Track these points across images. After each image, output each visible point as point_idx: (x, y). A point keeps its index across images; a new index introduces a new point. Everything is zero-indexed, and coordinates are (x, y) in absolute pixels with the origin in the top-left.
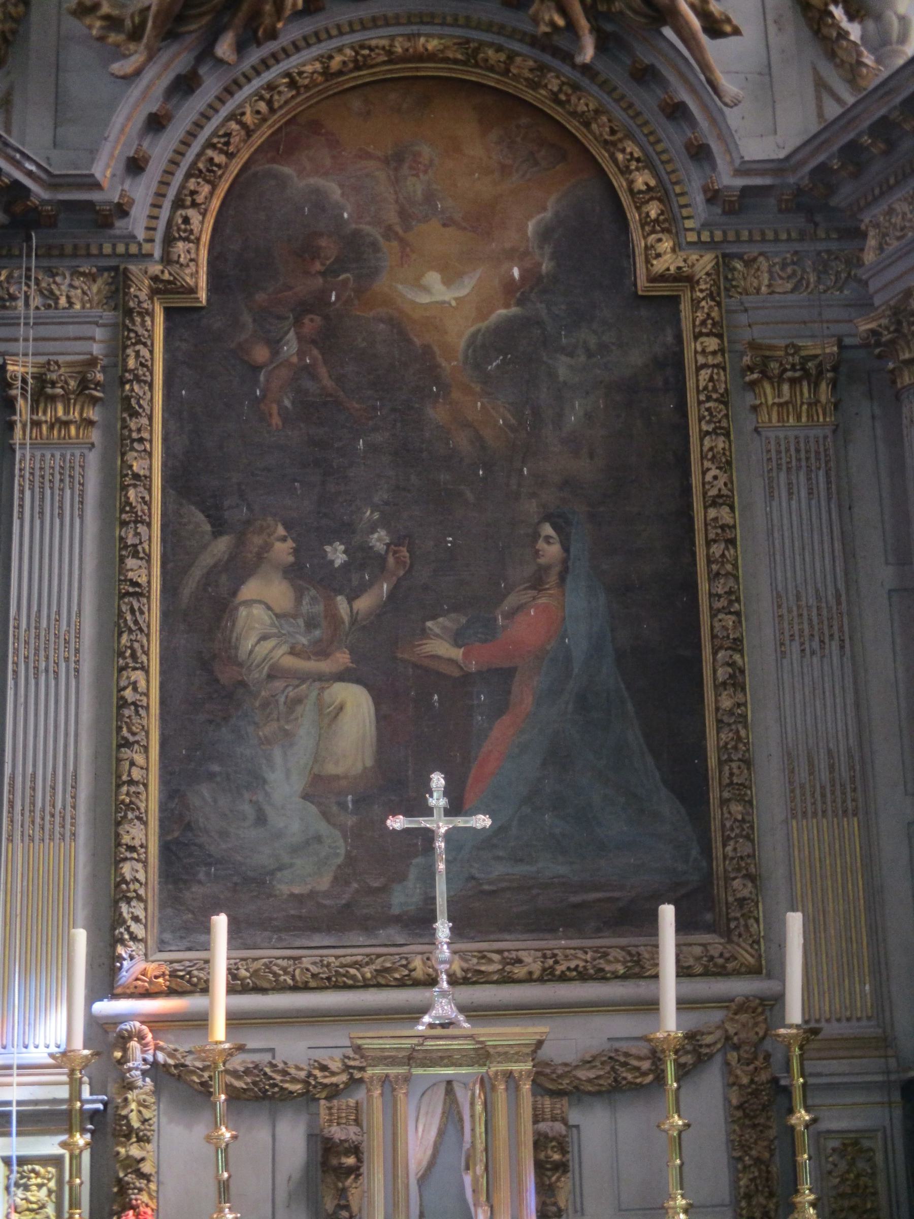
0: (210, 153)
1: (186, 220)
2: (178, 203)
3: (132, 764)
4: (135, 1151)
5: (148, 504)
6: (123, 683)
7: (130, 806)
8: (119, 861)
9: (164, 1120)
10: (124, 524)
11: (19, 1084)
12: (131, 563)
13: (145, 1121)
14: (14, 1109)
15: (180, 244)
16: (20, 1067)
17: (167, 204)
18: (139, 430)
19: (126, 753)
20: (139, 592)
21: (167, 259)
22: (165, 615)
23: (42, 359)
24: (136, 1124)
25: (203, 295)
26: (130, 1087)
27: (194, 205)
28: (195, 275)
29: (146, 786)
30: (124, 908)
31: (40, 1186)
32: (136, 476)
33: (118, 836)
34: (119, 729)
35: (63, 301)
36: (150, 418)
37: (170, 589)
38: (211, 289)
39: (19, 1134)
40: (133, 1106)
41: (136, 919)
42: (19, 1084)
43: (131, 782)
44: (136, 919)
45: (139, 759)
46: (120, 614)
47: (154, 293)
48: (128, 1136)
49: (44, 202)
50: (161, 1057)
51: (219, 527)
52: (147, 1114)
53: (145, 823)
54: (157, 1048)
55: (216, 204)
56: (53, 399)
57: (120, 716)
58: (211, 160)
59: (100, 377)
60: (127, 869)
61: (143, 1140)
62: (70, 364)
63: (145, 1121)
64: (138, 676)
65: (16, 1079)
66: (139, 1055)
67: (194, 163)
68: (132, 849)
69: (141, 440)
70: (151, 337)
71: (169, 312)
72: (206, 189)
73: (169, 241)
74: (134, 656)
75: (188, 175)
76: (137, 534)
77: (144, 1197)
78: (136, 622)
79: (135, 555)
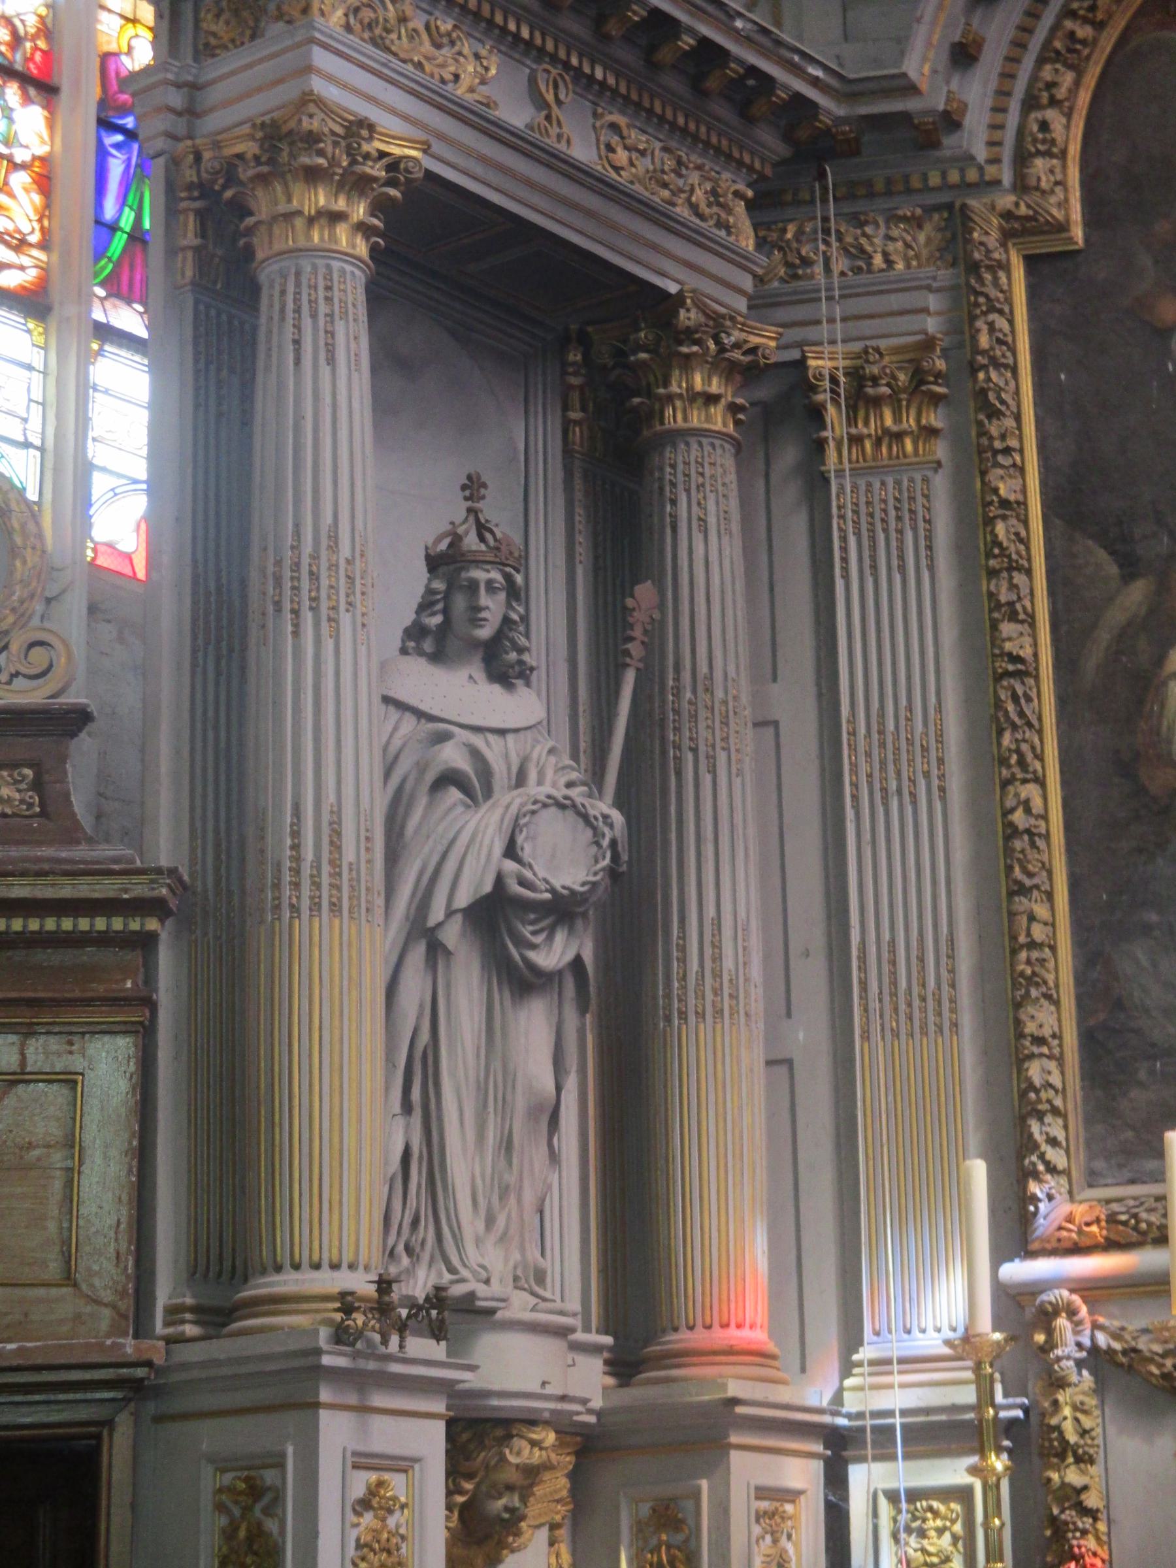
0: (1069, 24)
1: (1044, 126)
2: (1030, 103)
3: (1032, 918)
4: (1073, 1477)
5: (1026, 542)
6: (1010, 802)
7: (1033, 980)
8: (1021, 1060)
9: (1111, 1430)
10: (993, 573)
11: (903, 1386)
12: (1007, 628)
13: (1084, 1433)
14: (898, 1421)
15: (1039, 162)
16: (902, 1361)
17: (1015, 106)
18: (1003, 437)
19: (1022, 903)
20: (1023, 670)
21: (1022, 186)
22: (1062, 701)
23: (857, 347)
24: (1072, 1438)
25: (1078, 233)
26: (1061, 1383)
27: (1054, 102)
28: (1064, 204)
29: (1053, 948)
30: (1035, 1127)
31: (940, 1531)
32: (1005, 503)
33: (1018, 1022)
34: (1009, 869)
35: (878, 260)
36: (1018, 418)
37: (1065, 664)
38: (1087, 224)
39: (907, 1456)
40: (1067, 1411)
41: (1053, 1142)
42: (903, 1386)
43: (1032, 945)
44: (1053, 1142)
45: (1041, 911)
46: (998, 704)
47: (1007, 236)
48: (1062, 1456)
49: (839, 121)
50: (1102, 1339)
51: (1130, 568)
52: (1087, 1423)
53: (1057, 1003)
54: (1096, 1326)
55: (1084, 98)
56: (876, 402)
57: (1008, 851)
58: (1072, 35)
59: (940, 364)
60: (1035, 1070)
61: (1084, 1460)
62: (897, 350)
63: (1084, 1433)
64: (1030, 791)
65: (897, 1379)
66: (1070, 1337)
67: (1048, 43)
68: (1040, 1041)
69: (1007, 451)
70: (1009, 301)
71: (1031, 262)
72: (1068, 78)
73: (1022, 159)
74: (1022, 763)
75: (1041, 61)
76: (1013, 587)
77: (1091, 1543)
78: (1022, 714)
79: (1013, 617)
